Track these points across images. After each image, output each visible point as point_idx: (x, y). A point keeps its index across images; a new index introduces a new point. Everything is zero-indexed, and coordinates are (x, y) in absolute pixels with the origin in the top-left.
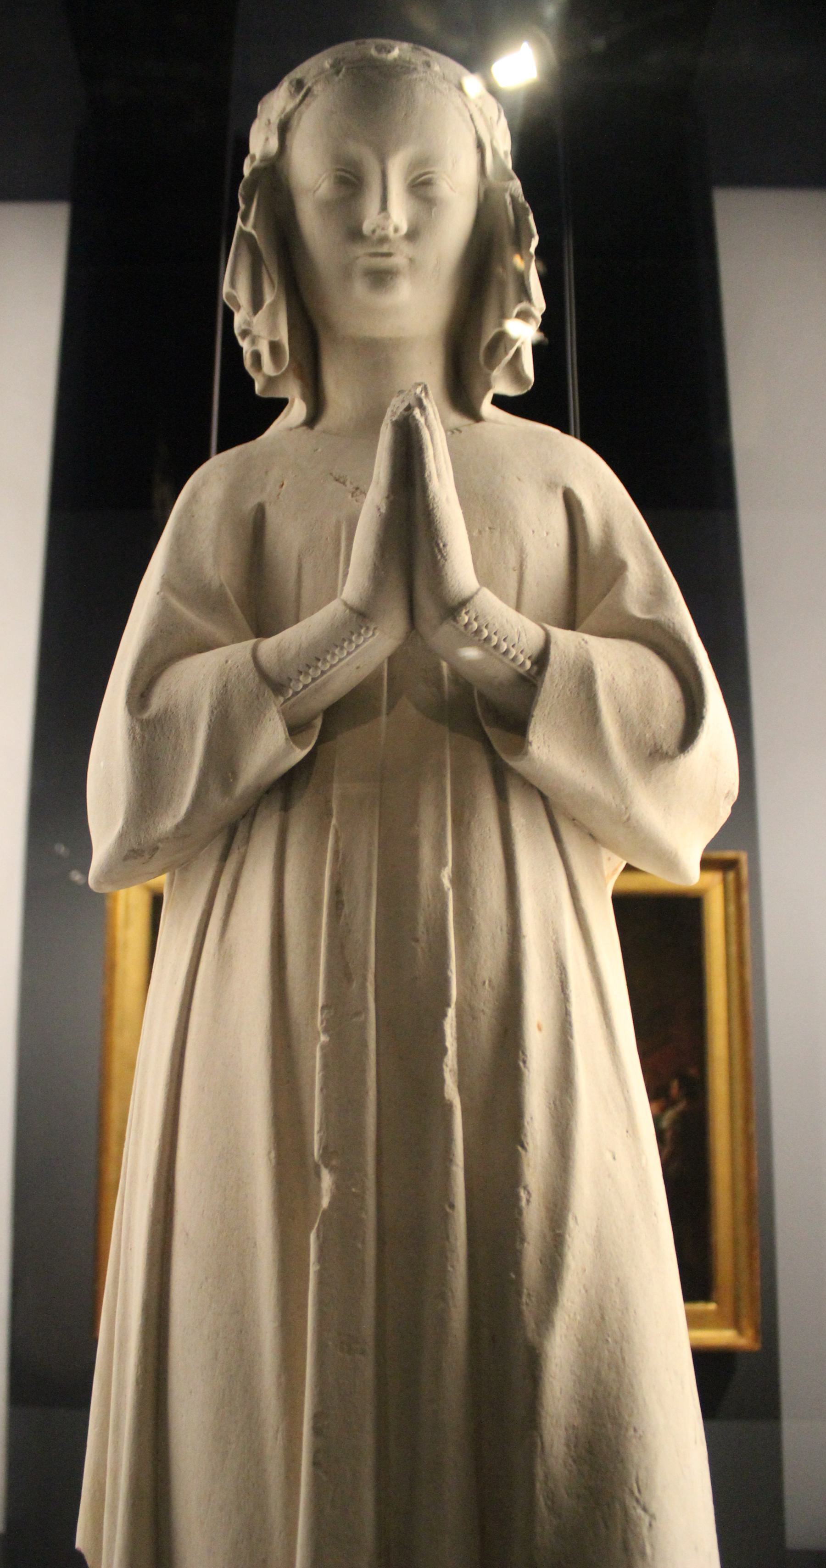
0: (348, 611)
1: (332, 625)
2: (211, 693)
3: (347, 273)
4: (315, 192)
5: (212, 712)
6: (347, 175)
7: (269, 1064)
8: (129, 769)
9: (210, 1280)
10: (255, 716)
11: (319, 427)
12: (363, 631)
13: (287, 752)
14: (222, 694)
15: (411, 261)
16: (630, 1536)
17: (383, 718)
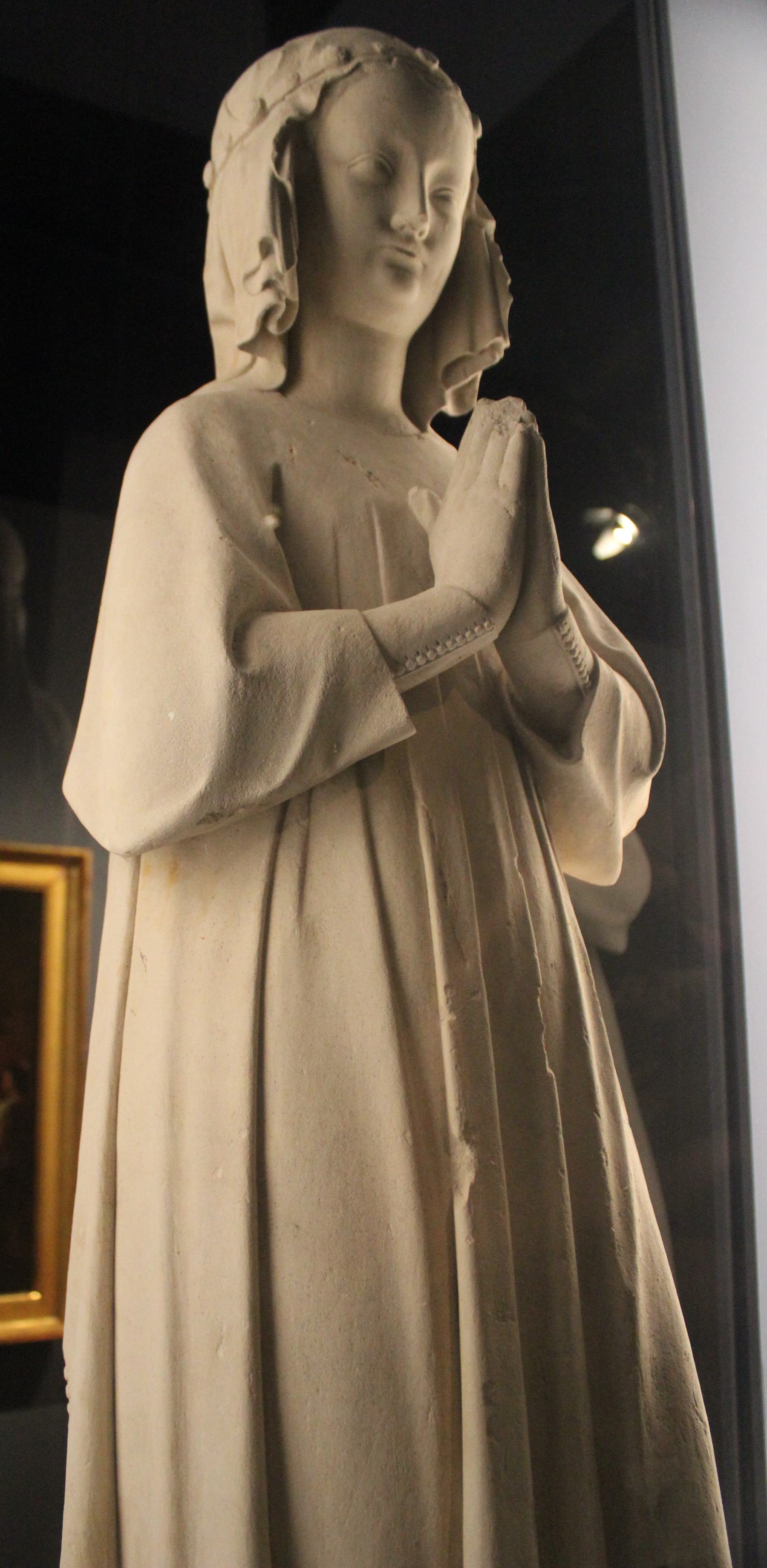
0: (474, 602)
1: (458, 612)
2: (326, 657)
3: (369, 258)
4: (350, 167)
5: (328, 679)
6: (387, 165)
7: (395, 1044)
8: (224, 726)
9: (335, 1271)
10: (371, 687)
11: (299, 394)
12: (486, 624)
13: (404, 731)
14: (338, 662)
15: (425, 266)
16: (699, 1444)
17: (442, 707)
